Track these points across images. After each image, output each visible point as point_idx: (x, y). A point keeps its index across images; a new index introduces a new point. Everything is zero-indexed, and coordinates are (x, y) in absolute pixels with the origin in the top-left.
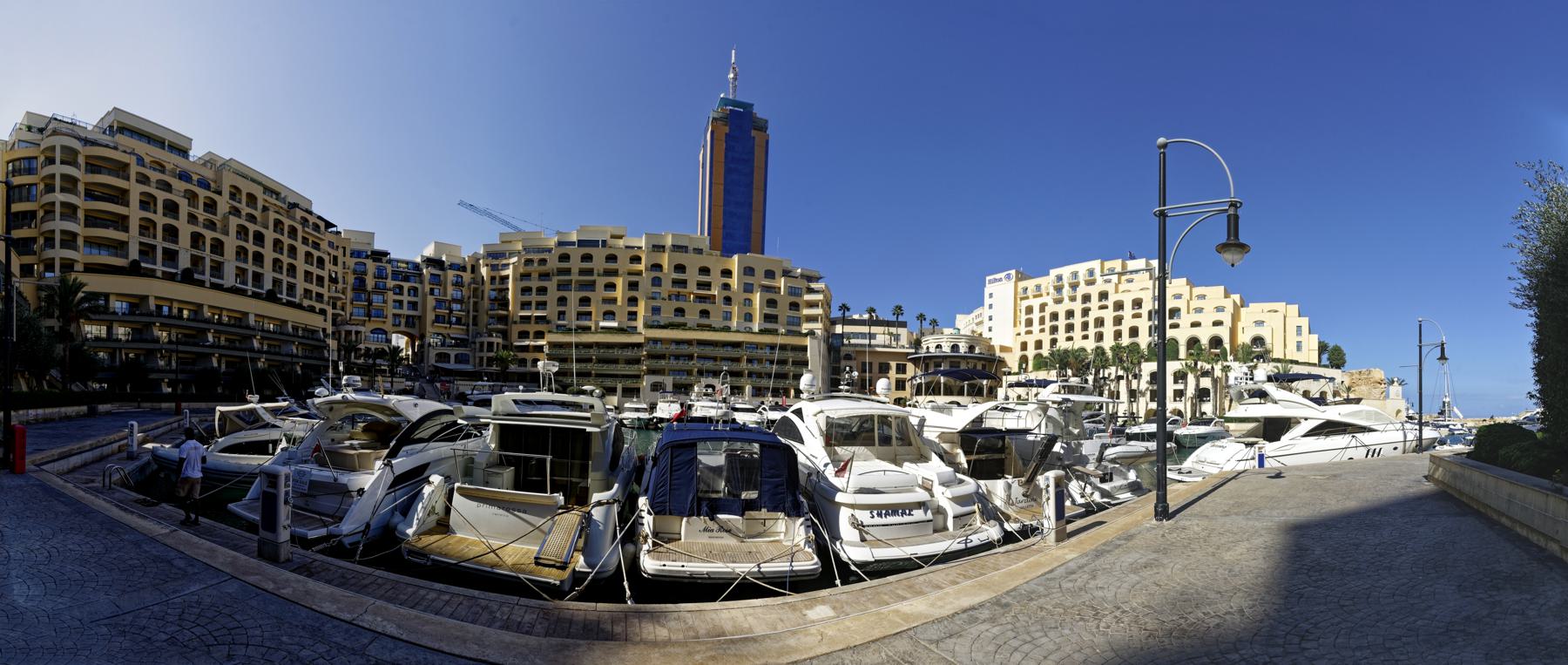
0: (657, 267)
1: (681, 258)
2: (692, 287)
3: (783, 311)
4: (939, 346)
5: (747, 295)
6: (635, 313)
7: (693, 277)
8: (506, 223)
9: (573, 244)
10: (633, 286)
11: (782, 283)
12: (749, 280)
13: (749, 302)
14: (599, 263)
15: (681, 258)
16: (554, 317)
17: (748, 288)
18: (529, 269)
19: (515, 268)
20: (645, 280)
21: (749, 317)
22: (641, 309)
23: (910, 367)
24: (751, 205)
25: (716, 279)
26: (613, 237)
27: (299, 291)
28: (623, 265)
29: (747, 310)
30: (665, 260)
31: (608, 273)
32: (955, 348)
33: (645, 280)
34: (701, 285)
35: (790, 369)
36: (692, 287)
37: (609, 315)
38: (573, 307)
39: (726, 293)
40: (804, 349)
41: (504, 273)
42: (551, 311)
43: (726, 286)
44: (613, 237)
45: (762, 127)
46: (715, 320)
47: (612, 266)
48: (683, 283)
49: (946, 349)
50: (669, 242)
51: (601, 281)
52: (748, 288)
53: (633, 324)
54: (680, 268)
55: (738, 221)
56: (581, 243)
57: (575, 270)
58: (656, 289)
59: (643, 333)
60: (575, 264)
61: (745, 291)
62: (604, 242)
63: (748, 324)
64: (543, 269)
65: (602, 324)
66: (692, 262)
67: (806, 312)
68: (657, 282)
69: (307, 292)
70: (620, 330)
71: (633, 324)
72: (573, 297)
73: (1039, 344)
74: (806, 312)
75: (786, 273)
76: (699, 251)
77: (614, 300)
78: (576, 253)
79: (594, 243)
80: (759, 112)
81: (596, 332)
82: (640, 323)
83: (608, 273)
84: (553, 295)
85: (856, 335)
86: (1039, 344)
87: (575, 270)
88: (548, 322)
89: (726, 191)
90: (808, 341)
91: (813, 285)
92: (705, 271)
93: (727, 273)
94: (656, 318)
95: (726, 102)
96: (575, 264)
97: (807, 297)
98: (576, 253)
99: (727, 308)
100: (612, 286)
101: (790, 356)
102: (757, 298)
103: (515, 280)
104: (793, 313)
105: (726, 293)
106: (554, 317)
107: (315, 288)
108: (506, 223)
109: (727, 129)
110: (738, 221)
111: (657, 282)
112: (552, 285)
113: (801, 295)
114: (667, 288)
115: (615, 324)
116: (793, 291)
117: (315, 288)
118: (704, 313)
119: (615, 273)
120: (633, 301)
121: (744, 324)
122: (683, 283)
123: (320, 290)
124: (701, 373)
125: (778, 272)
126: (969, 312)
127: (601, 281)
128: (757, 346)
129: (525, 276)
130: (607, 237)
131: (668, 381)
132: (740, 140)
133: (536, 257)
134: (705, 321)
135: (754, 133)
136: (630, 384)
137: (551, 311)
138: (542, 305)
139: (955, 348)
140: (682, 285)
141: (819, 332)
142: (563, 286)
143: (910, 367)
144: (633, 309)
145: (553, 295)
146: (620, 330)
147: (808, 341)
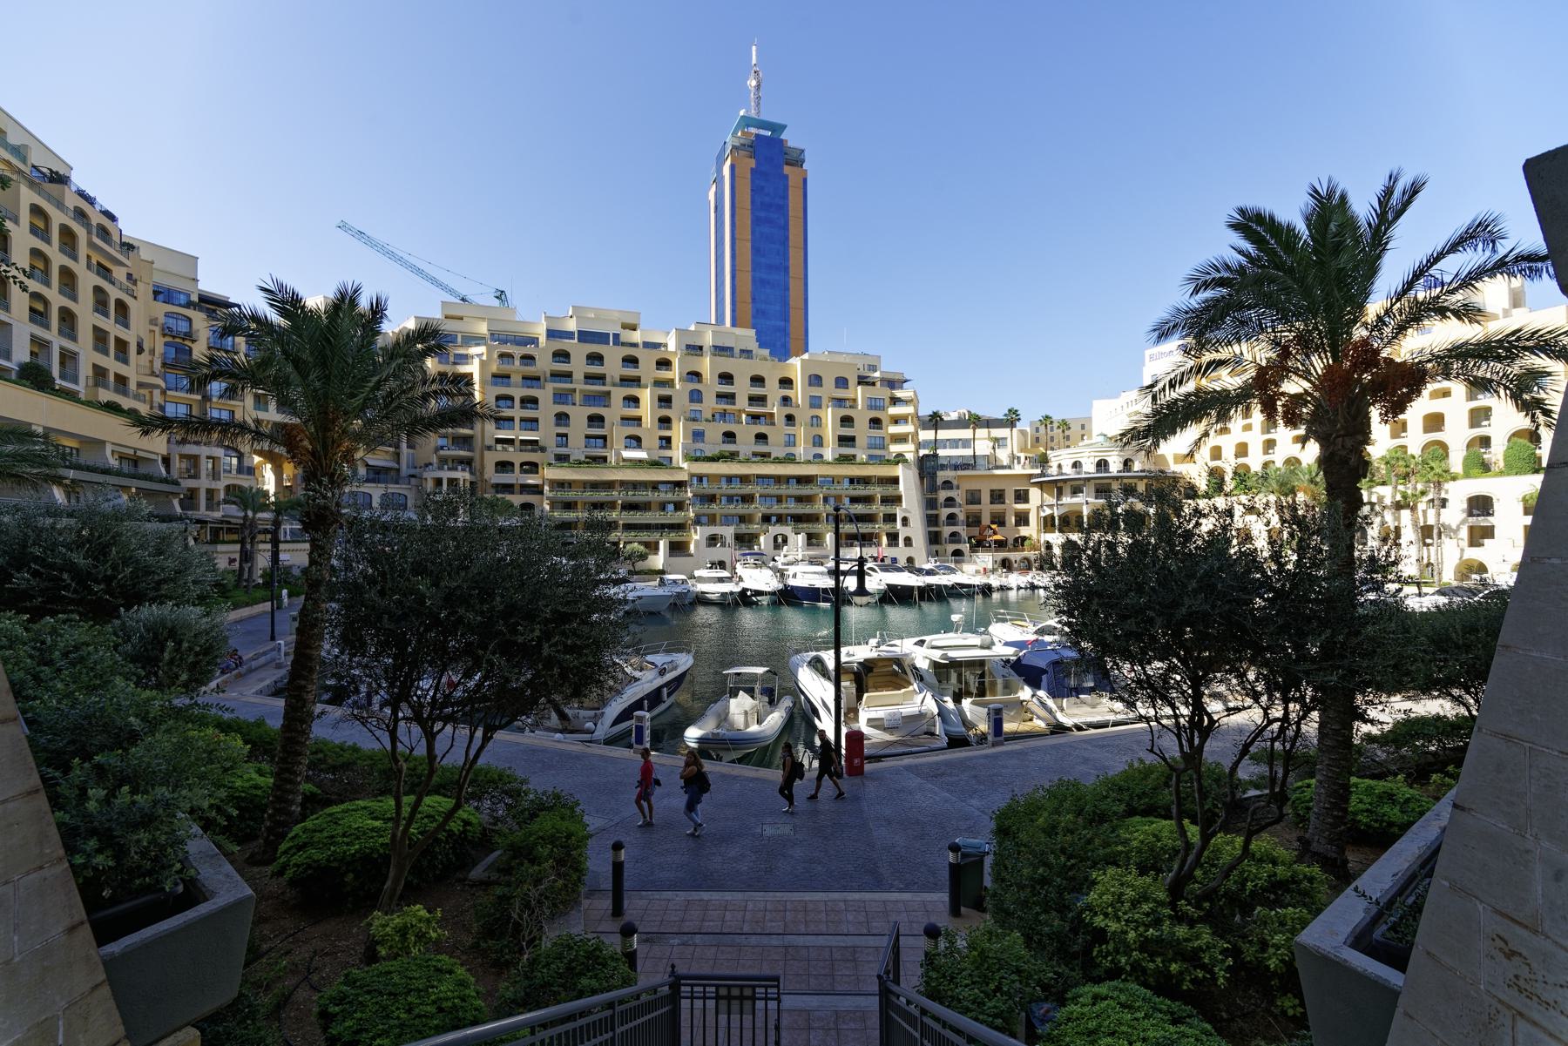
0: (696, 375)
1: (727, 365)
2: (742, 402)
3: (861, 430)
4: (1076, 465)
5: (816, 412)
6: (668, 440)
7: (742, 388)
8: (451, 291)
9: (570, 335)
10: (665, 401)
11: (860, 392)
12: (816, 391)
13: (817, 421)
14: (613, 366)
15: (727, 365)
16: (550, 441)
17: (815, 403)
18: (506, 368)
19: (483, 364)
20: (680, 388)
21: (818, 441)
22: (678, 433)
23: (1035, 494)
24: (787, 269)
25: (773, 391)
26: (625, 326)
27: (85, 371)
28: (647, 370)
29: (816, 431)
30: (706, 365)
31: (626, 381)
32: (1102, 465)
33: (680, 388)
34: (754, 400)
35: (878, 509)
36: (742, 402)
37: (636, 441)
38: (578, 427)
39: (788, 410)
40: (895, 481)
41: (463, 369)
42: (545, 433)
43: (786, 400)
44: (625, 326)
45: (797, 160)
46: (778, 451)
47: (630, 372)
48: (730, 397)
49: (1089, 468)
50: (708, 340)
51: (618, 393)
52: (815, 403)
53: (667, 453)
54: (726, 378)
55: (771, 287)
56: (585, 336)
57: (578, 376)
58: (696, 407)
59: (685, 468)
60: (578, 366)
61: (812, 406)
62: (616, 336)
63: (818, 450)
64: (530, 370)
65: (627, 454)
66: (742, 370)
67: (893, 429)
68: (696, 397)
69: (100, 373)
70: (655, 464)
71: (667, 453)
72: (579, 414)
73: (1242, 450)
74: (893, 429)
75: (863, 381)
76: (747, 353)
77: (638, 420)
78: (579, 351)
79: (602, 338)
80: (791, 139)
81: (617, 467)
82: (677, 453)
83: (626, 381)
84: (547, 410)
85: (955, 443)
86: (1242, 450)
87: (578, 376)
88: (543, 449)
89: (756, 251)
90: (899, 471)
91: (899, 394)
92: (758, 380)
93: (786, 382)
94: (700, 445)
95: (747, 122)
96: (578, 366)
97: (893, 411)
98: (579, 351)
99: (790, 430)
100: (634, 401)
101: (878, 491)
102: (829, 416)
103: (483, 382)
104: (876, 433)
105: (788, 410)
106: (550, 441)
107: (111, 364)
108: (451, 291)
109: (752, 163)
110: (771, 287)
111: (696, 397)
112: (545, 394)
113: (884, 409)
114: (710, 404)
115: (641, 455)
116: (873, 404)
117: (111, 364)
118: (761, 437)
119: (636, 381)
120: (665, 422)
121: (812, 447)
122: (730, 397)
123: (123, 370)
124: (766, 519)
125: (853, 381)
126: (1117, 396)
127: (618, 393)
128: (834, 480)
129: (501, 378)
130: (618, 330)
131: (728, 532)
132: (769, 178)
133: (518, 351)
134: (762, 449)
135: (787, 169)
136: (674, 537)
137: (545, 433)
138: (530, 423)
139: (1102, 465)
140: (739, 406)
141: (910, 457)
142: (561, 397)
143: (1035, 494)
144: (666, 433)
145: (547, 410)
146: (655, 464)
147: (899, 471)
